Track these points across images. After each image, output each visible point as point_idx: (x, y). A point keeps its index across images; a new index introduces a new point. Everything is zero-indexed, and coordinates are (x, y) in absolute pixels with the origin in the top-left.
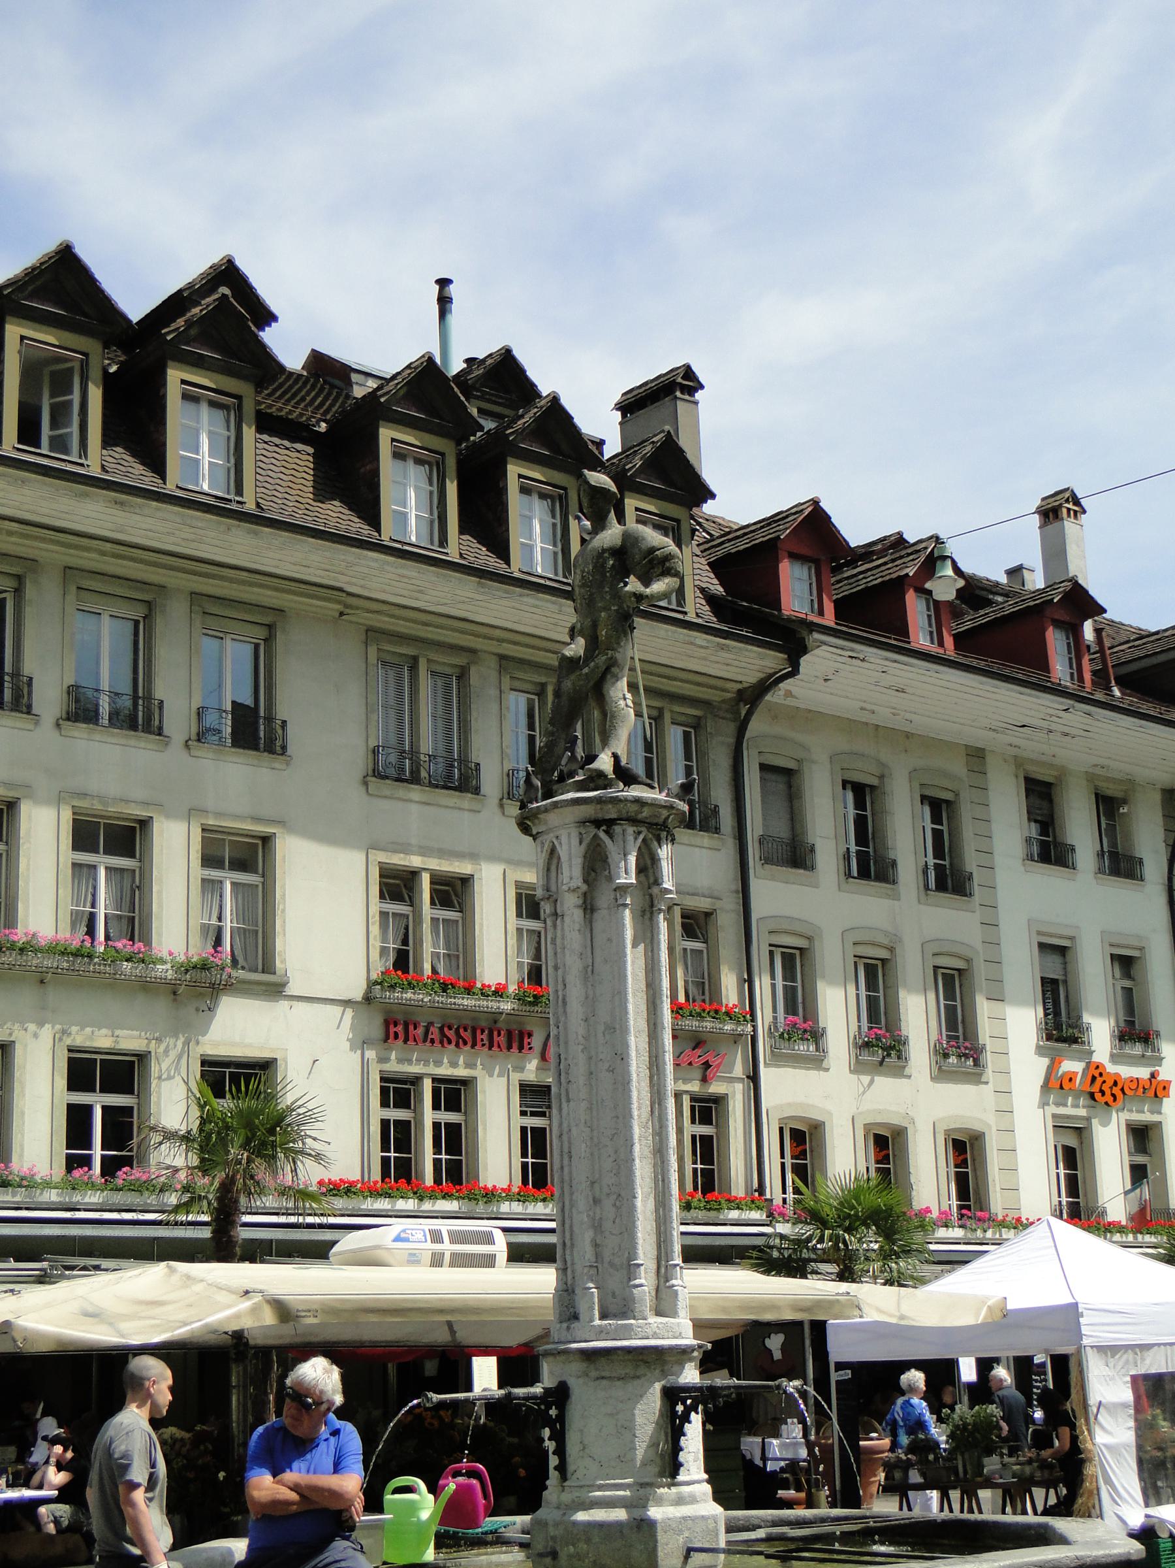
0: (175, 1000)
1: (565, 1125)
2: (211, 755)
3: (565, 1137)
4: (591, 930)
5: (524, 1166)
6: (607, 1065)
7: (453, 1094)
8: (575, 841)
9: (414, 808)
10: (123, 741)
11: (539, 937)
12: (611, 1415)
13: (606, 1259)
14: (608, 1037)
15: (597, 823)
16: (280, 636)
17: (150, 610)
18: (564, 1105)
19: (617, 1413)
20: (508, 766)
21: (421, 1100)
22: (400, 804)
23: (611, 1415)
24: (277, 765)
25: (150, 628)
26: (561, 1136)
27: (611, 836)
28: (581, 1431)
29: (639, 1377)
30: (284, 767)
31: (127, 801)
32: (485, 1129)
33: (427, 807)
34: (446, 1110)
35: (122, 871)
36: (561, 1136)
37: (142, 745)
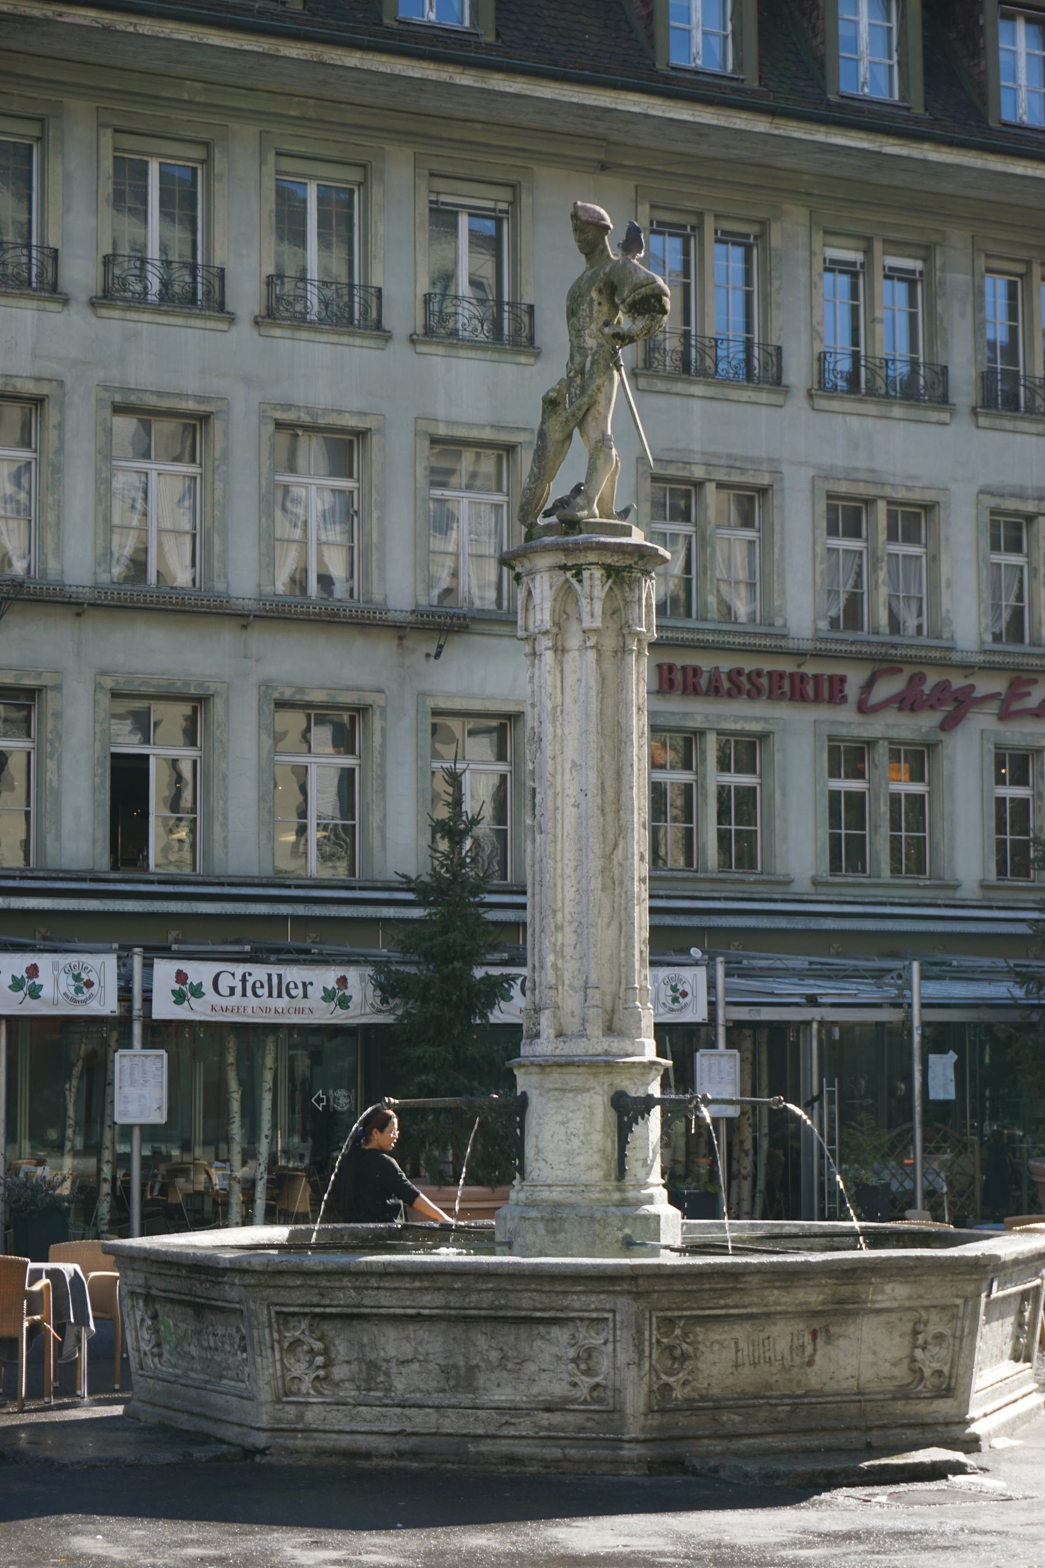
0: (400, 645)
1: (538, 855)
2: (441, 350)
3: (537, 867)
4: (562, 671)
5: (835, 840)
6: (573, 800)
7: (746, 751)
8: (547, 586)
9: (697, 405)
10: (335, 339)
11: (861, 558)
12: (563, 1123)
13: (567, 982)
14: (575, 774)
15: (564, 568)
16: (526, 200)
17: (366, 176)
18: (538, 837)
19: (568, 1121)
20: (818, 348)
21: (703, 760)
22: (678, 400)
23: (563, 1123)
24: (523, 359)
25: (366, 197)
26: (533, 866)
27: (580, 581)
28: (537, 1137)
29: (588, 1090)
30: (531, 360)
31: (340, 412)
32: (784, 794)
33: (715, 403)
34: (736, 772)
35: (341, 492)
36: (533, 866)
37: (358, 341)
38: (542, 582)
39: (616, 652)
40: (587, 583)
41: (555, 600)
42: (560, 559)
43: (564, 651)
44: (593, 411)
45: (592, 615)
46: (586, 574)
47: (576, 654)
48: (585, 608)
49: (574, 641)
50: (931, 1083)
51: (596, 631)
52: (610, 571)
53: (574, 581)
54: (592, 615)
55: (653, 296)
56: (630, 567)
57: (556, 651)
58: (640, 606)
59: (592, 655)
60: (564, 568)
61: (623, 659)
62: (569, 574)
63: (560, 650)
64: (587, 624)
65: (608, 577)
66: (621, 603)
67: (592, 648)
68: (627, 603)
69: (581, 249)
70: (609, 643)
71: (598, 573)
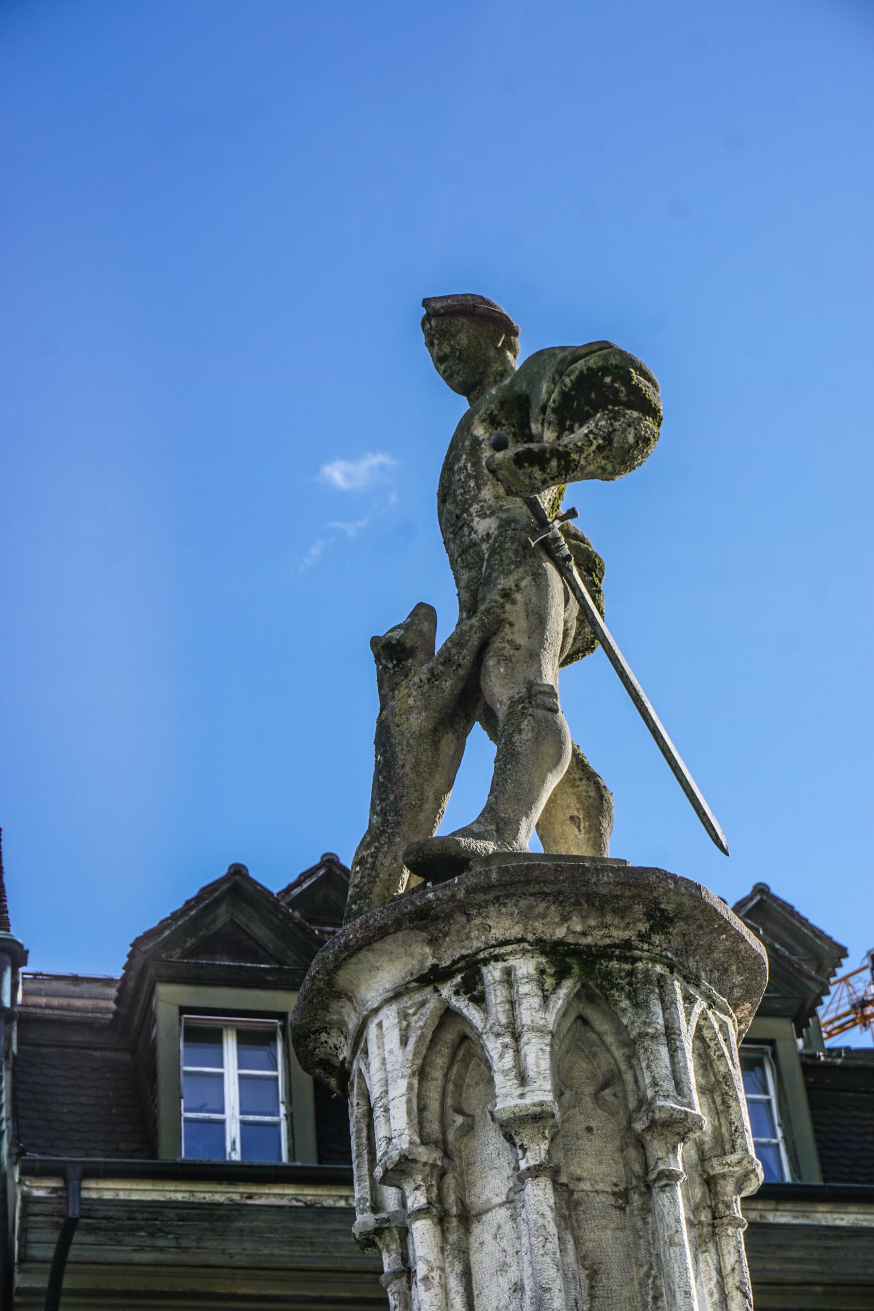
8: (393, 1038)
15: (432, 978)
27: (480, 1000)
38: (381, 1036)
39: (622, 1196)
40: (497, 996)
41: (422, 1073)
42: (420, 955)
43: (468, 1218)
44: (497, 643)
45: (523, 1079)
46: (493, 973)
47: (501, 1215)
48: (501, 1060)
49: (492, 1185)
50: (295, 1125)
51: (537, 1118)
52: (560, 958)
53: (461, 1004)
54: (523, 1079)
55: (605, 370)
56: (627, 944)
57: (442, 1220)
58: (674, 1051)
59: (539, 1196)
60: (432, 978)
61: (647, 1209)
62: (446, 990)
63: (457, 1218)
64: (508, 1098)
65: (561, 975)
66: (619, 1054)
67: (535, 1172)
68: (632, 1045)
69: (448, 378)
70: (597, 1167)
71: (525, 966)
